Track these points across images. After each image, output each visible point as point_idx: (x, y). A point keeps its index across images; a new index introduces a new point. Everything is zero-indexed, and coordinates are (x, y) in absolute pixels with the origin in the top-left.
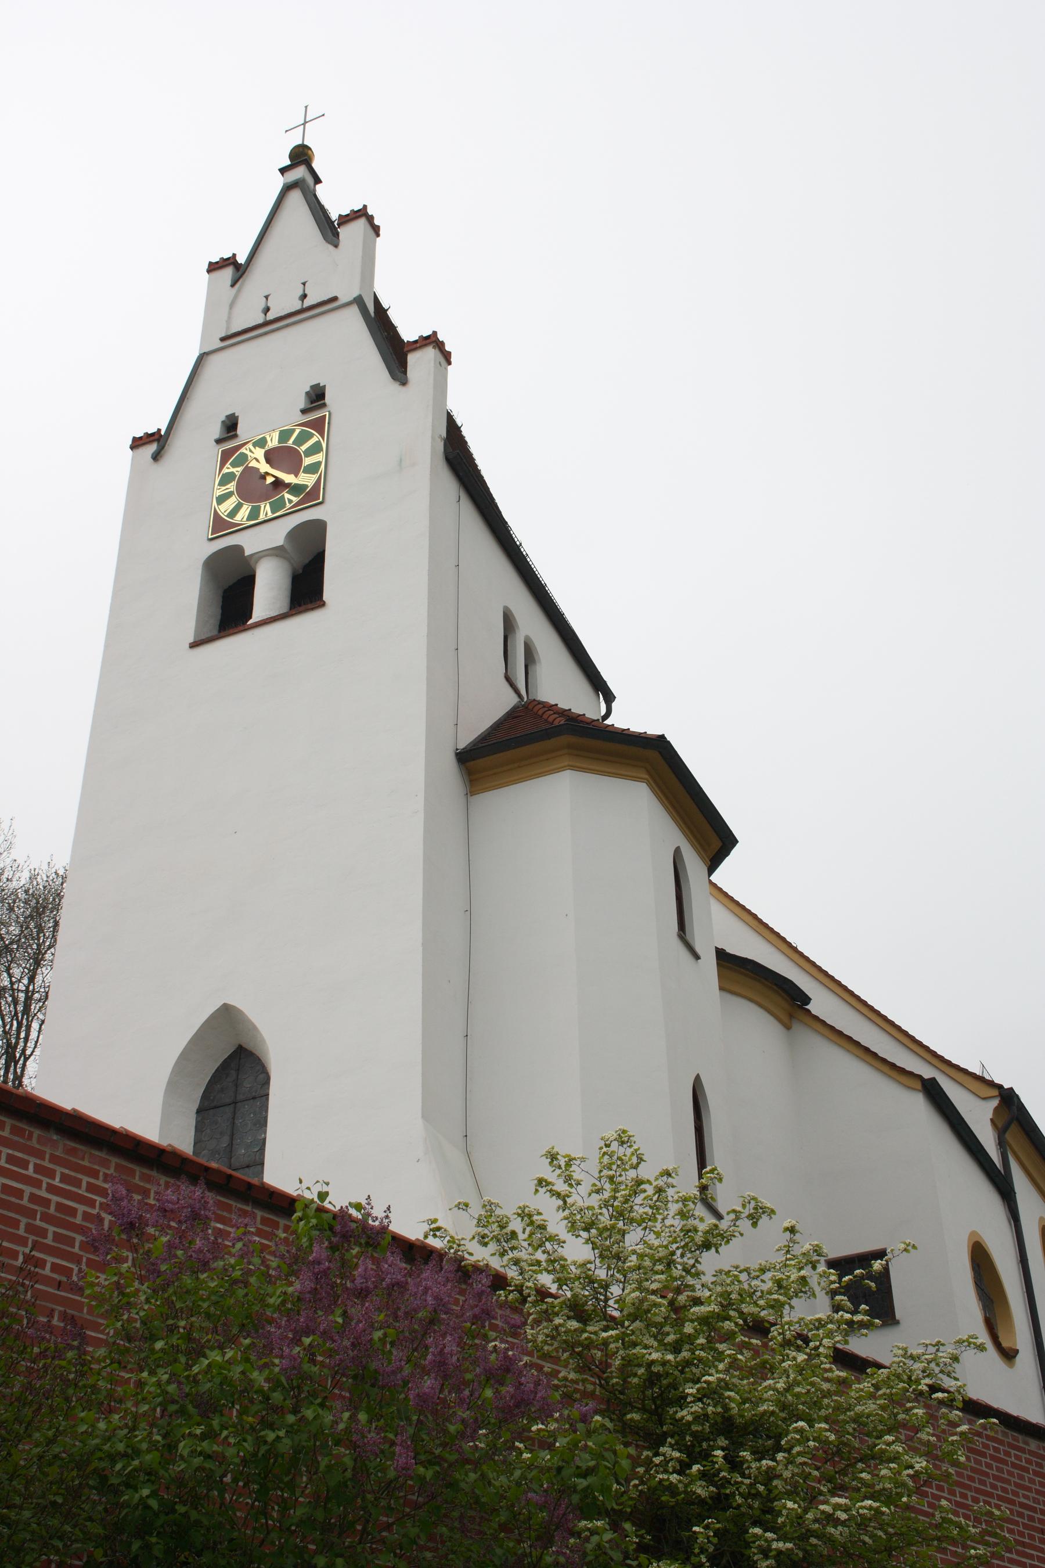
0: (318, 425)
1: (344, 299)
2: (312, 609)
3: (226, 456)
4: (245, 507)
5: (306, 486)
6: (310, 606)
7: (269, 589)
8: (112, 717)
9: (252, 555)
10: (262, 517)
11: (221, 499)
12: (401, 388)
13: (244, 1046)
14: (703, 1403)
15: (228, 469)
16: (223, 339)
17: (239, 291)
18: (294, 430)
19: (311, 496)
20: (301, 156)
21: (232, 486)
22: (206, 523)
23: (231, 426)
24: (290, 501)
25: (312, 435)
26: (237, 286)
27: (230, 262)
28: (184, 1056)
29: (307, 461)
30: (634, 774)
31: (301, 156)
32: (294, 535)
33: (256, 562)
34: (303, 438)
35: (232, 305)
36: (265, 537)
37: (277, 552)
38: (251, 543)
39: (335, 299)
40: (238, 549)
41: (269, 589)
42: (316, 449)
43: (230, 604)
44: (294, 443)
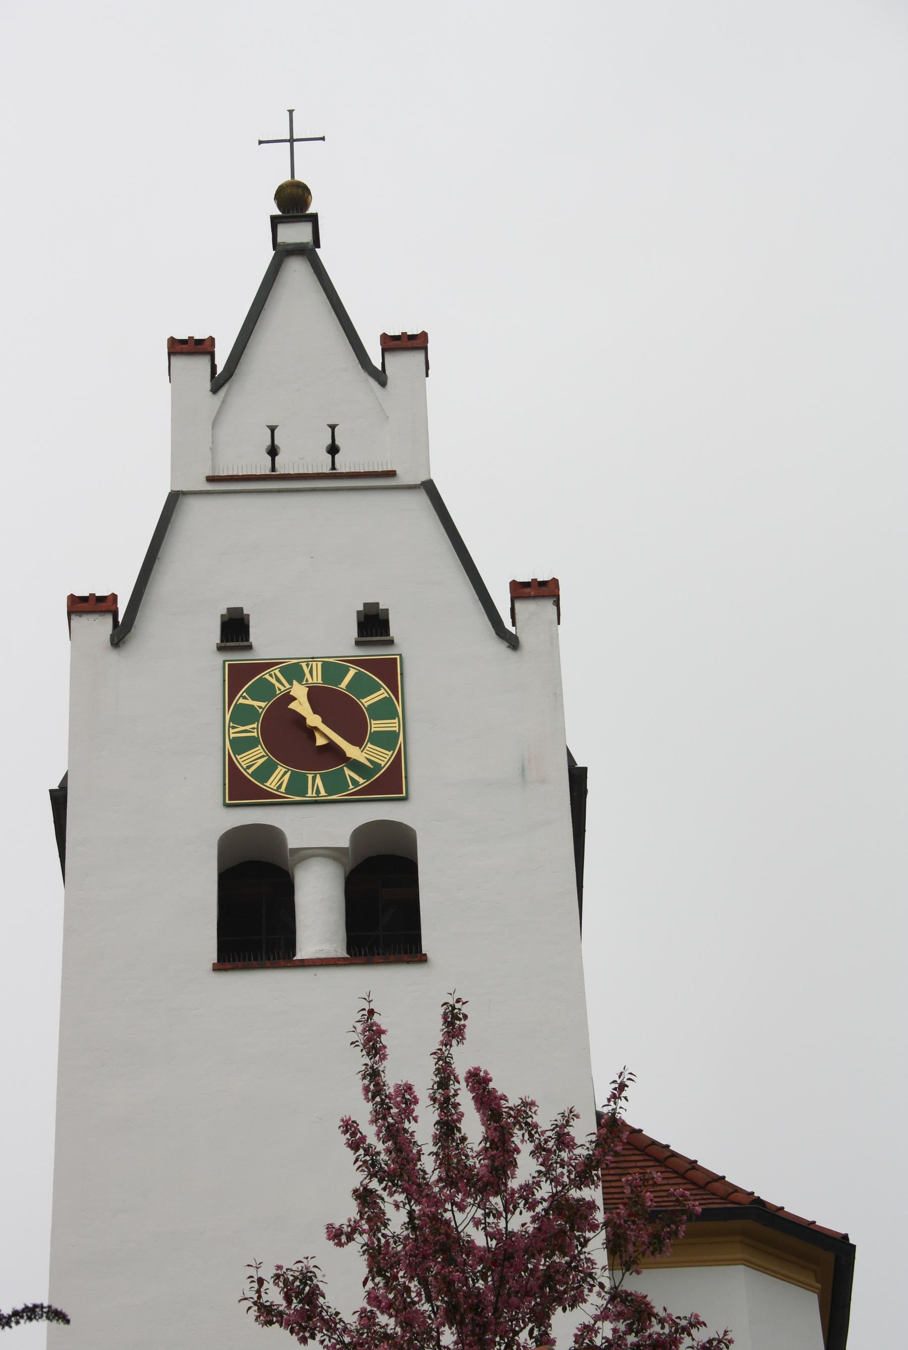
0: (388, 671)
1: (405, 478)
2: (408, 962)
3: (238, 676)
4: (281, 770)
5: (377, 766)
6: (405, 957)
7: (318, 909)
8: (90, 1053)
9: (295, 851)
11: (241, 745)
12: (509, 652)
15: (244, 699)
16: (211, 479)
18: (347, 670)
19: (390, 783)
20: (293, 202)
21: (253, 730)
23: (235, 629)
24: (355, 783)
26: (222, 393)
27: (201, 347)
32: (362, 834)
33: (295, 865)
34: (362, 686)
35: (215, 423)
36: (318, 828)
37: (334, 854)
39: (391, 474)
40: (273, 835)
41: (318, 909)
42: (385, 710)
43: (252, 917)
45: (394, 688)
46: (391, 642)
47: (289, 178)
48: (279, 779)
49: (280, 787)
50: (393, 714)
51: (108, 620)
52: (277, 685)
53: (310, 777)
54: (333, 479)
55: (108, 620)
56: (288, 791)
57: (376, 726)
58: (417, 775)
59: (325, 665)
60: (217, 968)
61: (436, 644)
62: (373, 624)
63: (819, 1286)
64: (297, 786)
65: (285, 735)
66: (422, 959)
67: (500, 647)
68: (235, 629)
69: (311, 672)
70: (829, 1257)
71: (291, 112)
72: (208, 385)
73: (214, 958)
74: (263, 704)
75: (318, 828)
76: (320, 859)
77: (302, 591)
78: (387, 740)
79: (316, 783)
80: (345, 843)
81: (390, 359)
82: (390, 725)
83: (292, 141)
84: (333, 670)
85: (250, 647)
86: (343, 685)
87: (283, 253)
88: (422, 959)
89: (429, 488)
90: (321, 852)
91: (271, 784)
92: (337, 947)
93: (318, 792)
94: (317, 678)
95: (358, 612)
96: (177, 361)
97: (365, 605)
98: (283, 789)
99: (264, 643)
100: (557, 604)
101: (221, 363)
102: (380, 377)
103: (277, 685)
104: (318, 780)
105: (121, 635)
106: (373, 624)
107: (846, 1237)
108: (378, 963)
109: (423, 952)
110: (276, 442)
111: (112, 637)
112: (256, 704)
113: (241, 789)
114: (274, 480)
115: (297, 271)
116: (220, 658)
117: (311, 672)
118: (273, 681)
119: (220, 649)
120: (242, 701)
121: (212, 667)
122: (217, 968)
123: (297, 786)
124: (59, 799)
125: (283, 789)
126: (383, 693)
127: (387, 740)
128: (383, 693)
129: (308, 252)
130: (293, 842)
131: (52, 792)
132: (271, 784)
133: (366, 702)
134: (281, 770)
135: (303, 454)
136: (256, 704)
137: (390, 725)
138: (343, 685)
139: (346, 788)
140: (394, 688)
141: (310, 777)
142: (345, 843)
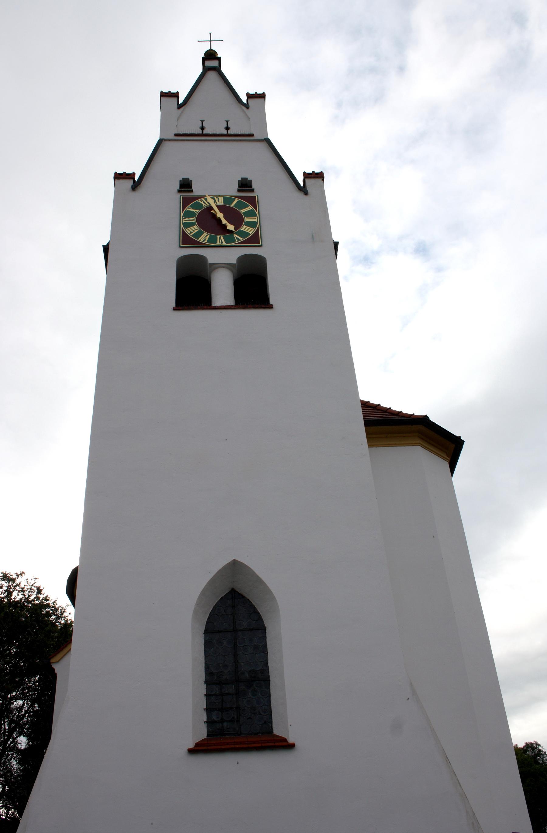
0: (253, 201)
1: (257, 136)
3: (186, 202)
4: (205, 234)
5: (249, 234)
6: (263, 306)
7: (223, 288)
9: (211, 265)
10: (218, 243)
11: (187, 225)
12: (304, 196)
13: (236, 589)
14: (11, 759)
15: (189, 209)
16: (176, 135)
17: (182, 112)
18: (234, 200)
19: (255, 240)
20: (210, 55)
21: (193, 220)
22: (175, 237)
23: (185, 185)
24: (238, 240)
25: (248, 206)
26: (182, 109)
28: (203, 593)
29: (196, 211)
30: (414, 442)
31: (210, 55)
32: (242, 259)
34: (241, 205)
36: (222, 258)
37: (229, 266)
38: (212, 256)
39: (252, 135)
40: (202, 259)
41: (223, 288)
42: (251, 214)
43: (192, 290)
44: (234, 206)
45: (255, 206)
46: (253, 191)
47: (209, 49)
48: (205, 237)
49: (205, 240)
50: (255, 215)
51: (132, 181)
52: (204, 204)
53: (218, 237)
54: (227, 135)
55: (132, 181)
56: (208, 242)
57: (247, 219)
58: (266, 236)
59: (224, 198)
60: (175, 309)
61: (271, 198)
62: (245, 185)
63: (449, 459)
64: (213, 240)
65: (208, 220)
66: (271, 307)
67: (300, 195)
68: (185, 185)
69: (218, 200)
70: (452, 446)
71: (210, 34)
72: (176, 106)
73: (174, 305)
74: (197, 211)
75: (222, 258)
76: (225, 269)
77: (215, 189)
78: (252, 225)
79: (221, 239)
80: (234, 261)
81: (250, 100)
82: (254, 219)
83: (210, 41)
84: (228, 200)
85: (192, 191)
86: (233, 205)
87: (206, 70)
88: (271, 307)
89: (268, 141)
90: (223, 265)
91: (201, 239)
92: (231, 301)
93: (222, 242)
94: (221, 202)
95: (239, 181)
96: (163, 98)
97: (241, 178)
98: (206, 241)
99: (197, 190)
100: (323, 180)
101: (181, 101)
102: (247, 106)
103: (204, 204)
104: (222, 238)
105: (136, 186)
106: (245, 185)
107: (460, 437)
108: (250, 308)
109: (271, 304)
110: (204, 125)
111: (132, 186)
112: (194, 211)
113: (187, 241)
114: (202, 135)
115: (212, 75)
116: (179, 195)
117: (218, 200)
118: (202, 203)
119: (179, 191)
120: (188, 209)
121: (176, 199)
122: (175, 309)
123: (213, 240)
124: (106, 249)
125: (206, 241)
126: (250, 208)
127: (252, 225)
128: (250, 208)
129: (218, 70)
130: (210, 261)
131: (104, 246)
132: (201, 239)
133: (243, 211)
134: (205, 234)
135: (215, 126)
136: (194, 211)
137: (254, 219)
138: (233, 205)
139: (235, 241)
140: (255, 206)
141: (218, 237)
142: (234, 261)
